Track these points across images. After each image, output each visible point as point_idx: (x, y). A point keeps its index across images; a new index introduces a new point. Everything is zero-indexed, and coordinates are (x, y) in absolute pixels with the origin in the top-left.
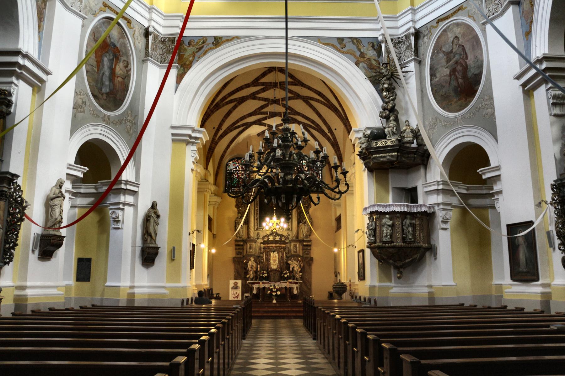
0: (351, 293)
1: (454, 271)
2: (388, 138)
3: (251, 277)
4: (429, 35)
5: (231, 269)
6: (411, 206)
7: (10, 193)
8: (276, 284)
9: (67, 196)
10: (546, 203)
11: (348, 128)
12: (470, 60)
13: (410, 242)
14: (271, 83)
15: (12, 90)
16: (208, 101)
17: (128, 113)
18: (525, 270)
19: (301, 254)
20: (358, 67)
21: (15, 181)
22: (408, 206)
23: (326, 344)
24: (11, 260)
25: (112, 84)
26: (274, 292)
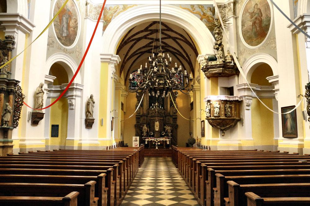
0: (198, 144)
1: (252, 132)
2: (217, 60)
3: (145, 135)
4: (241, 3)
5: (133, 131)
6: (230, 97)
7: (16, 91)
8: (158, 139)
9: (45, 92)
10: (302, 96)
11: (197, 54)
12: (264, 17)
13: (229, 117)
14: (155, 30)
15: (15, 36)
16: (120, 40)
17: (77, 47)
18: (290, 132)
19: (172, 123)
21: (18, 84)
22: (228, 97)
23: (182, 170)
24: (17, 126)
25: (68, 31)
26: (157, 143)
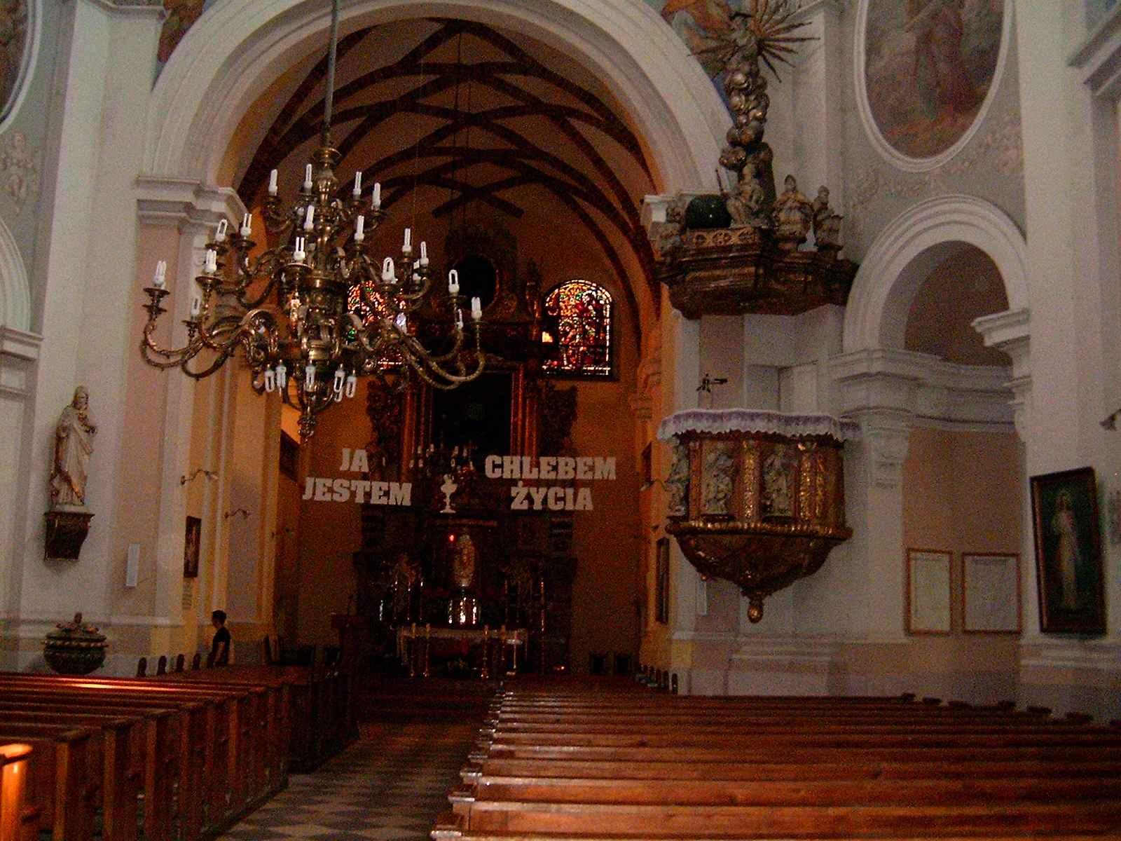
2: (733, 225)
13: (784, 521)
20: (669, 23)
